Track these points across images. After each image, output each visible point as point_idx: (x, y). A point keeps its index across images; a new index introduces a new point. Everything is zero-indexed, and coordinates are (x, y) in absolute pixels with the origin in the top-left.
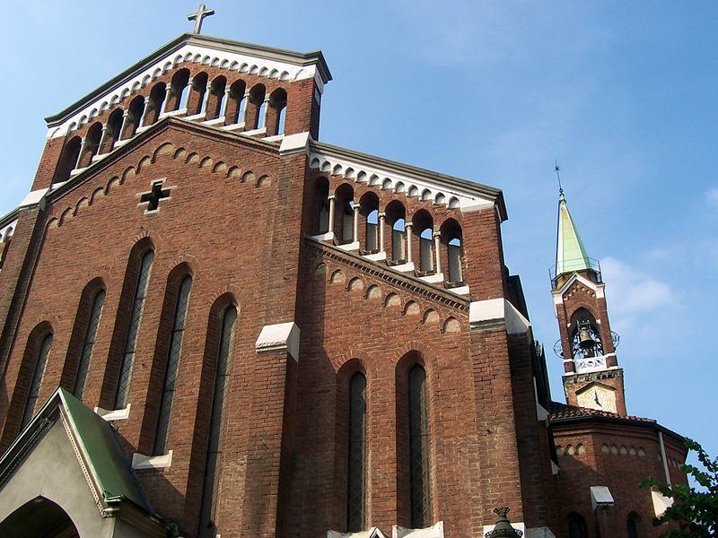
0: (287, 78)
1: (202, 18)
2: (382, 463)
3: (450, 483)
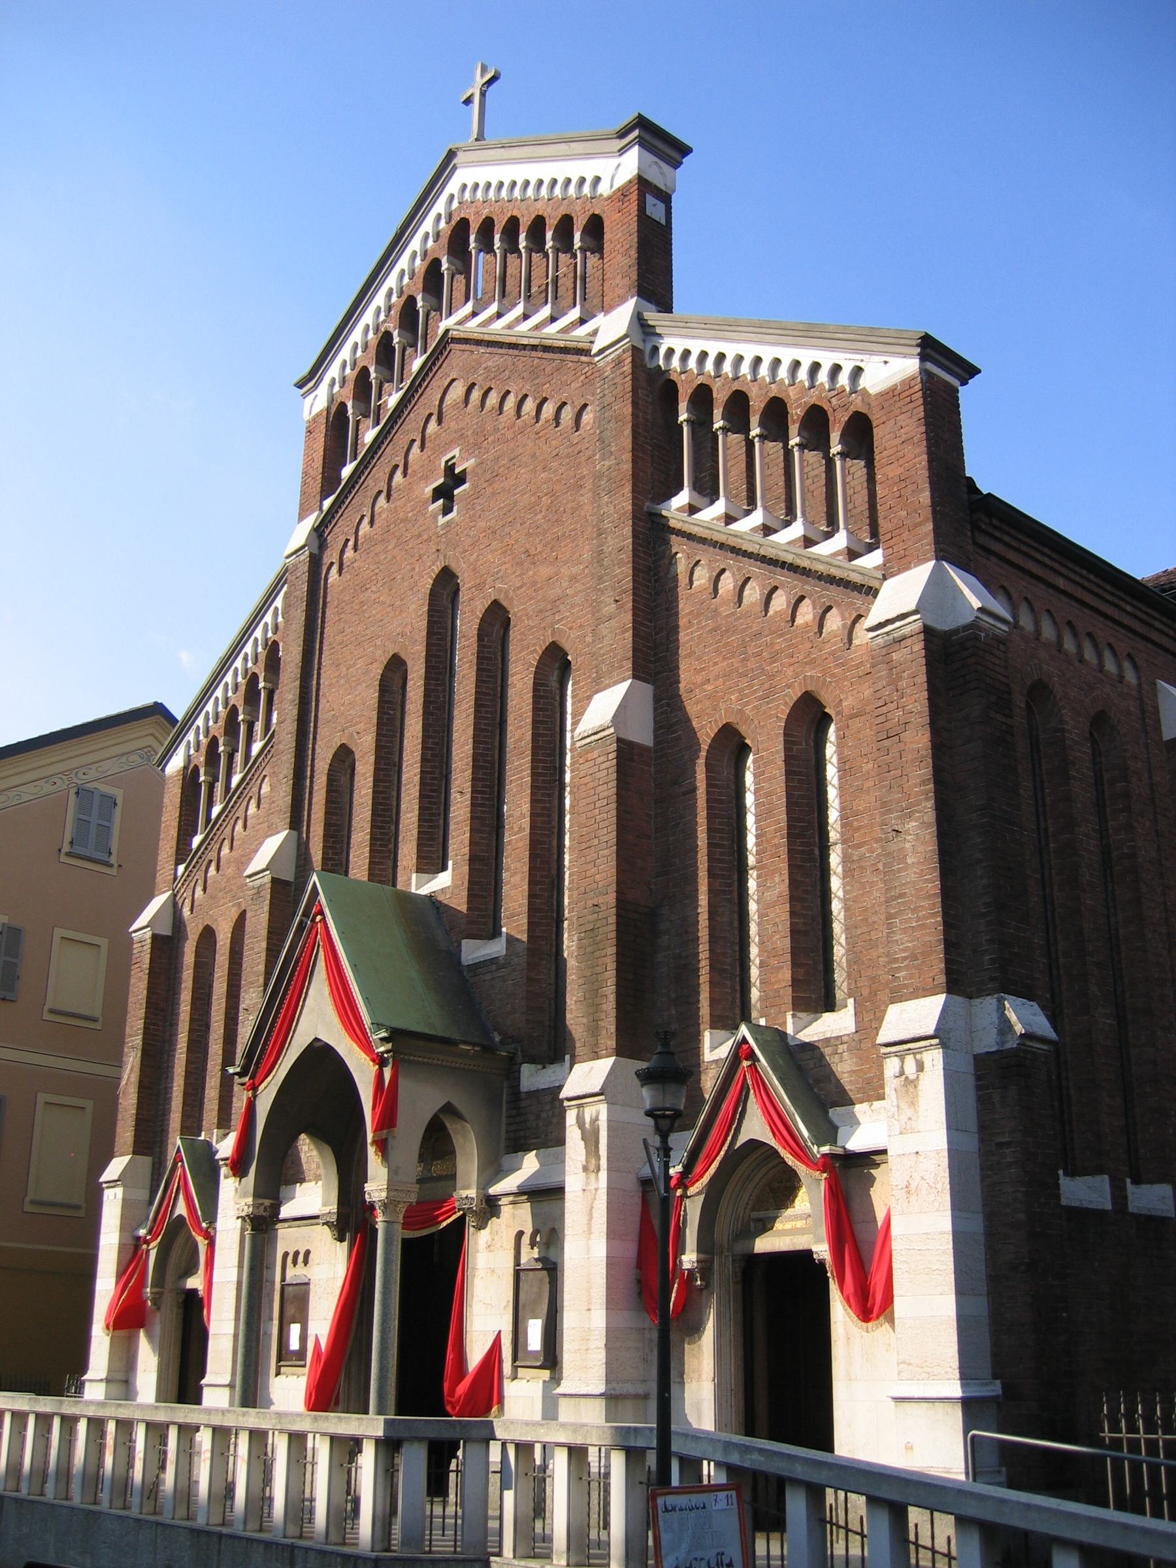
1: (483, 94)
3: (864, 929)
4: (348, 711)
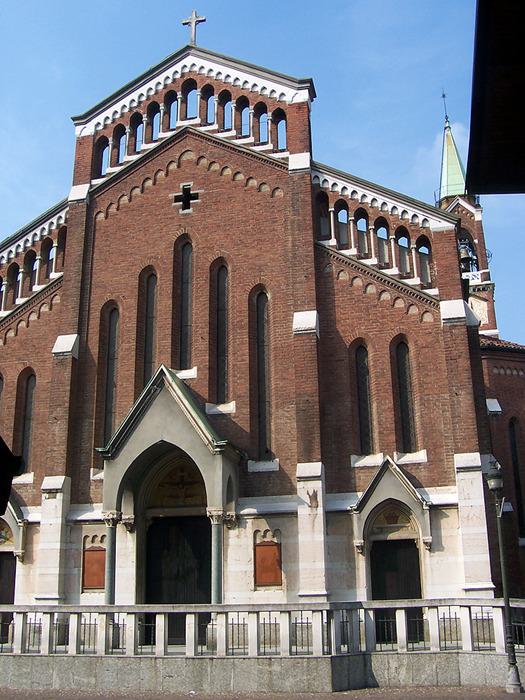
0: (284, 99)
2: (384, 411)
4: (115, 281)
